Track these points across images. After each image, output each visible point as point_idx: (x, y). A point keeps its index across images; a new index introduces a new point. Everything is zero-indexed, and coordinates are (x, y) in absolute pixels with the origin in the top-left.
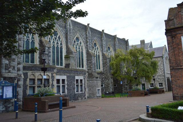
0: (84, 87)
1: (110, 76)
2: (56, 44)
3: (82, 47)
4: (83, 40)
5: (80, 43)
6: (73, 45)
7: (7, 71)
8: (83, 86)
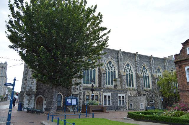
0: (126, 101)
1: (158, 94)
2: (110, 70)
4: (133, 65)
5: (130, 68)
7: (74, 91)
8: (125, 101)
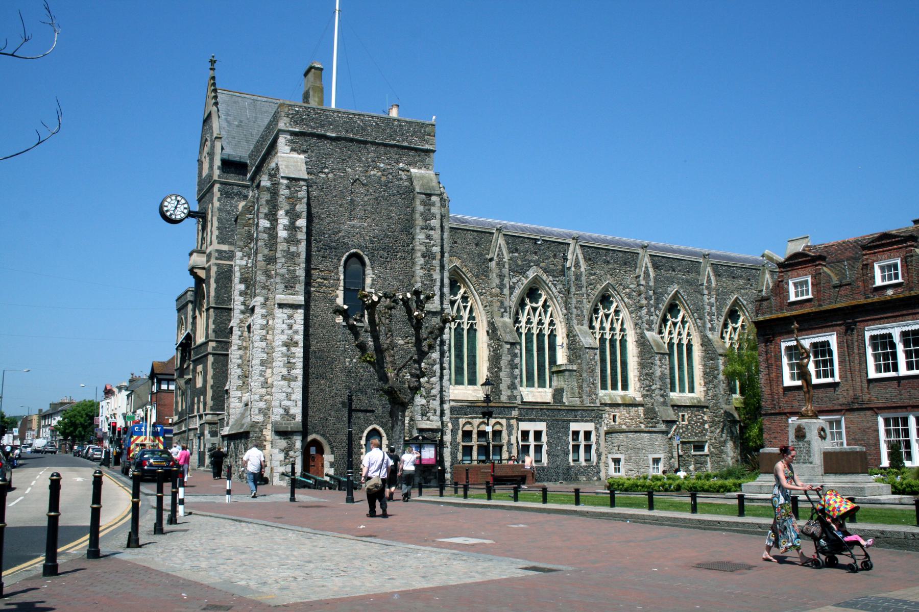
0: (597, 450)
2: (534, 325)
3: (622, 324)
4: (626, 300)
6: (591, 321)
7: (425, 418)
8: (594, 448)
